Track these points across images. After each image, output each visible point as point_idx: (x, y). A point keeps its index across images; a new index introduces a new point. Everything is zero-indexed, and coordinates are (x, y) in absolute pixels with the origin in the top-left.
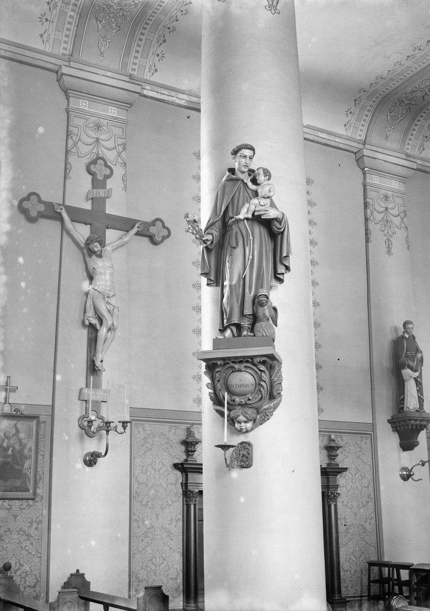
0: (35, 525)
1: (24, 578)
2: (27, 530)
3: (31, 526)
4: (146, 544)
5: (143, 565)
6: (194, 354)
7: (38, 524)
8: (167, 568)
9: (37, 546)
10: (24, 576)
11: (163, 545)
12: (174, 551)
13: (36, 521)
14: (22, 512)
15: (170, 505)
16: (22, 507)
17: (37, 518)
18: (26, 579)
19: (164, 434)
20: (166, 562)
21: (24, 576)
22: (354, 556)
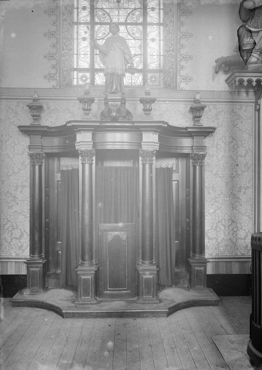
0: (20, 189)
1: (11, 231)
2: (237, 194)
3: (16, 190)
4: (216, 208)
5: (213, 225)
6: (46, 35)
7: (246, 189)
8: (12, 228)
9: (21, 206)
10: (11, 230)
11: (8, 208)
12: (19, 214)
13: (244, 187)
14: (9, 178)
15: (16, 173)
16: (9, 174)
17: (245, 185)
18: (12, 232)
19: (11, 108)
20: (11, 223)
21: (11, 230)
22: (222, 225)
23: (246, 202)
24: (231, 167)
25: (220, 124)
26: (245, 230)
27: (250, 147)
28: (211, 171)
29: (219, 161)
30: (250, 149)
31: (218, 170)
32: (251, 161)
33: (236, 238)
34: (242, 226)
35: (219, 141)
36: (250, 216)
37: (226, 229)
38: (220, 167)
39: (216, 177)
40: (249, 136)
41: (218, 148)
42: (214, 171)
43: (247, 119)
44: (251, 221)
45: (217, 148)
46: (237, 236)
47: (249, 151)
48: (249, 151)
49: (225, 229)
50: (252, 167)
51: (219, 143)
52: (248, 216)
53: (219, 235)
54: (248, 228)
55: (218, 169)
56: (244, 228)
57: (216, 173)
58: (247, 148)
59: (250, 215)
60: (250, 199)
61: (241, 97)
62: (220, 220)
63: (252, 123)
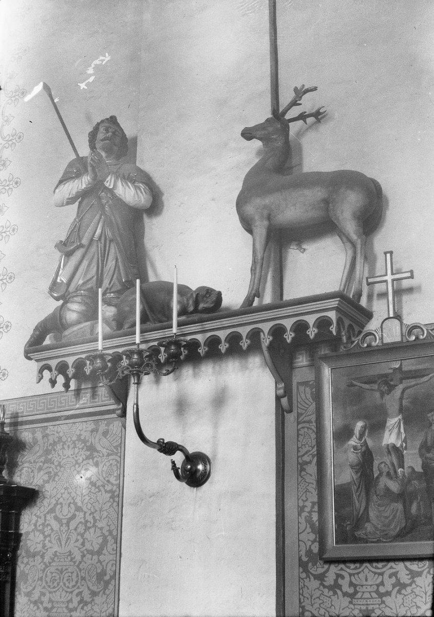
22: (56, 518)
23: (108, 455)
24: (69, 583)
25: (53, 473)
26: (101, 529)
27: (113, 527)
28: (28, 594)
29: (47, 567)
30: (110, 532)
31: (44, 590)
32: (112, 565)
33: (82, 550)
34: (98, 518)
35: (48, 517)
36: (115, 491)
37: (62, 528)
38: (47, 583)
39: (38, 608)
40: (111, 497)
41: (46, 534)
42: (36, 596)
43: (108, 455)
44: (115, 504)
45: (43, 533)
46: (84, 546)
47: (109, 538)
48: (109, 538)
49: (60, 529)
50: (114, 581)
51: (47, 522)
52: (111, 491)
53: (48, 545)
54: (109, 524)
55: (44, 587)
56: (99, 525)
57: (40, 598)
58: (105, 531)
59: (115, 488)
60: (117, 449)
61: (99, 399)
62: (52, 506)
63: (119, 465)
